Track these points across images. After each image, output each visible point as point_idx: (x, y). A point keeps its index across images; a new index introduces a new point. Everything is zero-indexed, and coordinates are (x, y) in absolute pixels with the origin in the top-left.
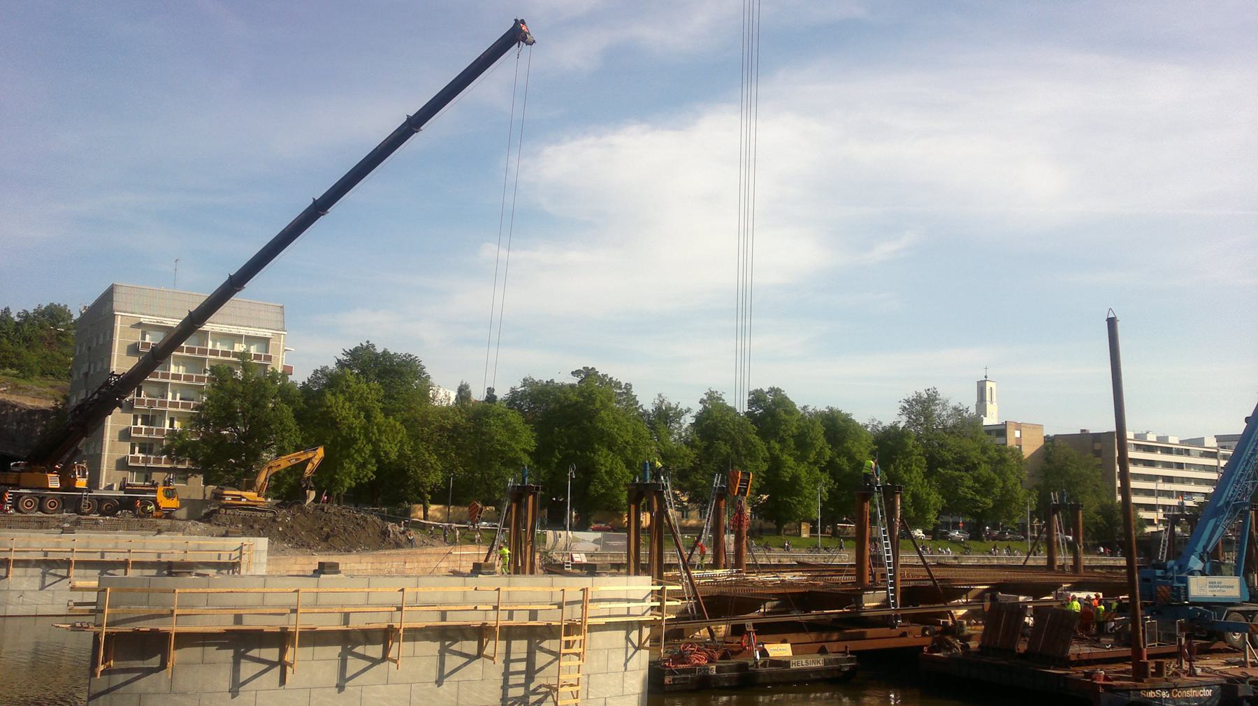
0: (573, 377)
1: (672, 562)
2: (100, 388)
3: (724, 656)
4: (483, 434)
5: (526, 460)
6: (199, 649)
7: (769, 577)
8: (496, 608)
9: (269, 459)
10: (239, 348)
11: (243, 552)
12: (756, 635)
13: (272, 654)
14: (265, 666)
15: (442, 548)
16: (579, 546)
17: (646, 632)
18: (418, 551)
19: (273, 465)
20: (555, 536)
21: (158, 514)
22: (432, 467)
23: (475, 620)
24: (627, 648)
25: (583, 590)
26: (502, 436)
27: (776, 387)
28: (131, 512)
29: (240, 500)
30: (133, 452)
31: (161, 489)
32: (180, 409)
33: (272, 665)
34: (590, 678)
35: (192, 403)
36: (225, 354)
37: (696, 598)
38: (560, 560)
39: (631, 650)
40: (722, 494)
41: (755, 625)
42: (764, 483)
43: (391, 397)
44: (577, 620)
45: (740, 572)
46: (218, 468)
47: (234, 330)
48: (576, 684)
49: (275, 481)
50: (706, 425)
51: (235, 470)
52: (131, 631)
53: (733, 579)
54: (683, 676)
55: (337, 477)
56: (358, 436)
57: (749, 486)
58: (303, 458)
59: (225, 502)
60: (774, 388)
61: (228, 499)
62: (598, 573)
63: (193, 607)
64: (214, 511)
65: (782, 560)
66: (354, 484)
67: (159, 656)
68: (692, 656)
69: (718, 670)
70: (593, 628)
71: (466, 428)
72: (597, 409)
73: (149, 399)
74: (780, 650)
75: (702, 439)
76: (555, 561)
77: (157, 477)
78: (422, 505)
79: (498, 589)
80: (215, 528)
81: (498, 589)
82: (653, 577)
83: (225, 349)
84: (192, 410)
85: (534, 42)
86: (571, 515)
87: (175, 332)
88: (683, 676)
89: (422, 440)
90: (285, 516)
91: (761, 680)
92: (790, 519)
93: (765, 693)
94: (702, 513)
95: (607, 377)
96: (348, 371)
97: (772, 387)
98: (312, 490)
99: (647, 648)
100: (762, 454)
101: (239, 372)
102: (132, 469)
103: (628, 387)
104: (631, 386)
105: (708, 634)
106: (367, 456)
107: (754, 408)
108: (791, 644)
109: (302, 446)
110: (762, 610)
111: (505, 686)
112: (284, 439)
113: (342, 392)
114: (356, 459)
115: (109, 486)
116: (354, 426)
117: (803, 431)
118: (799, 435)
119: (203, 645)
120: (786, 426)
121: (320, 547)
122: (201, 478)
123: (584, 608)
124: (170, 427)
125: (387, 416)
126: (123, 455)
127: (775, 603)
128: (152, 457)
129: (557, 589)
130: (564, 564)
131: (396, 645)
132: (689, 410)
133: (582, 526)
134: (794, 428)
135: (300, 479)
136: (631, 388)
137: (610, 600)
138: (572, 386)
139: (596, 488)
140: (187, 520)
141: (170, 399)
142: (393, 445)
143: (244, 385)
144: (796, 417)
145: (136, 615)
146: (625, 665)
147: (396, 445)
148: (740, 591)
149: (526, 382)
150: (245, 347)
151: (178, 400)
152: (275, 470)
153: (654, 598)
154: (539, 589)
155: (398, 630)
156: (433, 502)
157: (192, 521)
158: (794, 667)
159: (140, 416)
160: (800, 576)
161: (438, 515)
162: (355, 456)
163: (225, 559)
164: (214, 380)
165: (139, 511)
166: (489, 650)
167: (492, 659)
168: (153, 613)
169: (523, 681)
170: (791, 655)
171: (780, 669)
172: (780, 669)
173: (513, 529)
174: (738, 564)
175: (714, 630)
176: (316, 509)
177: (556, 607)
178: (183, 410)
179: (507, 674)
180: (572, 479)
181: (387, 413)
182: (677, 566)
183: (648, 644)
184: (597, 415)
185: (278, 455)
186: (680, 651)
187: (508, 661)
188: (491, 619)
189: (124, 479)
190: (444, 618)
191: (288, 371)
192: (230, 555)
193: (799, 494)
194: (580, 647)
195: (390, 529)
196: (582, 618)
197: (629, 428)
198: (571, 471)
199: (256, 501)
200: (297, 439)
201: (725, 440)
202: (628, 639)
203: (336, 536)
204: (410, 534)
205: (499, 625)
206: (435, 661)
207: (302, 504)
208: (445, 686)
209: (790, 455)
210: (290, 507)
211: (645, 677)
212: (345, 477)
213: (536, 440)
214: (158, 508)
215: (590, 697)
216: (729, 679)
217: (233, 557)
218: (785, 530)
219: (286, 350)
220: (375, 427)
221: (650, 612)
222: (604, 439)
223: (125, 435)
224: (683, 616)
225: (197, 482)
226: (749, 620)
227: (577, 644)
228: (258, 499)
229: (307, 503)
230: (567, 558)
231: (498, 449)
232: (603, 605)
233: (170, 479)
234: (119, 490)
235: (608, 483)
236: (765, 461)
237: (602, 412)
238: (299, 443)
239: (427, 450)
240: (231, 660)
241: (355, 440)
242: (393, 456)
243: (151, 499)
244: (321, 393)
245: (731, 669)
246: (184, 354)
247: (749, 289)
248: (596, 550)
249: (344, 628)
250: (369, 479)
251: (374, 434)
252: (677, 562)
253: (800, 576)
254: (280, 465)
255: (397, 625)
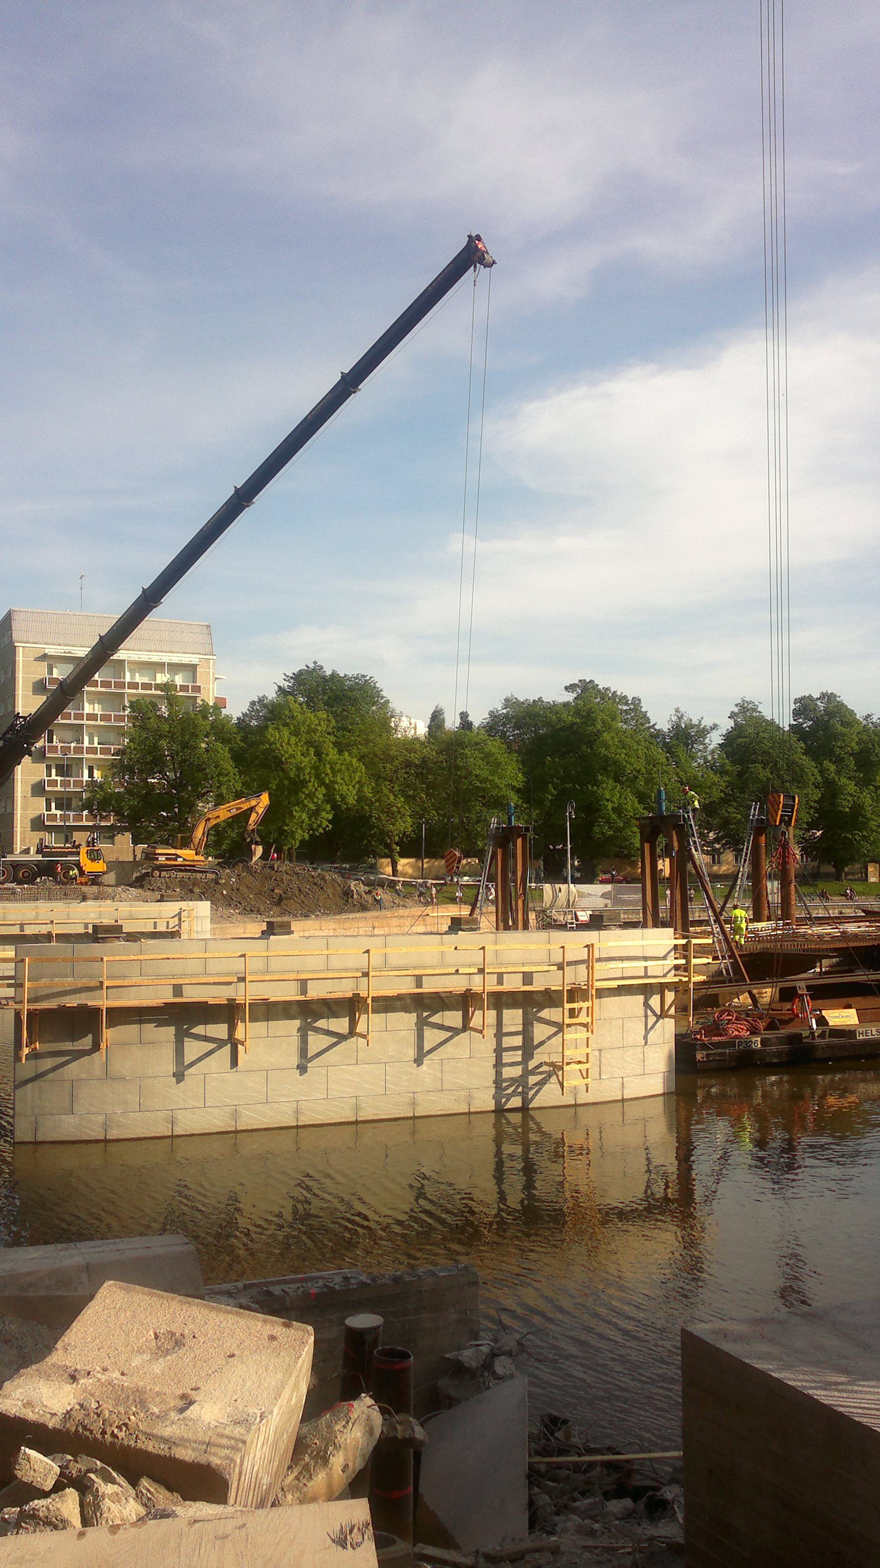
0: (567, 693)
1: (702, 918)
2: (5, 734)
3: (771, 1026)
4: (458, 768)
5: (514, 799)
6: (135, 1027)
7: (827, 930)
8: (481, 971)
9: (206, 810)
10: (162, 678)
11: (183, 919)
12: (811, 999)
13: (219, 1030)
14: (211, 1046)
15: (415, 909)
16: (585, 902)
17: (670, 996)
18: (388, 913)
19: (210, 816)
20: (554, 891)
21: (83, 880)
22: (399, 812)
23: (458, 985)
24: (646, 1016)
25: (587, 946)
26: (480, 769)
27: (829, 692)
28: (50, 878)
29: (176, 860)
30: (49, 808)
31: (83, 850)
32: (99, 756)
33: (221, 1043)
34: (603, 1054)
35: (112, 747)
36: (146, 686)
37: (732, 956)
38: (562, 919)
39: (652, 1019)
40: (761, 828)
41: (809, 988)
42: (816, 815)
43: (344, 729)
44: (582, 984)
45: (788, 924)
46: (147, 824)
47: (155, 657)
48: (585, 1061)
49: (215, 836)
50: (737, 745)
51: (167, 825)
52: (56, 1007)
53: (779, 932)
54: (719, 1051)
55: (286, 828)
56: (307, 778)
57: (795, 812)
58: (245, 806)
59: (158, 863)
60: (827, 693)
61: (162, 859)
62: (605, 926)
63: (124, 977)
64: (147, 874)
65: (844, 911)
66: (307, 837)
67: (90, 1036)
68: (729, 1026)
69: (763, 1042)
70: (601, 993)
71: (438, 762)
72: (598, 731)
73: (62, 745)
74: (843, 1016)
75: (734, 763)
76: (555, 921)
77: (80, 837)
78: (389, 860)
79: (483, 948)
80: (149, 893)
81: (483, 948)
82: (675, 930)
83: (146, 680)
84: (113, 755)
85: (494, 262)
86: (572, 863)
87: (86, 661)
88: (719, 1051)
89: (385, 779)
90: (229, 877)
91: (819, 1054)
92: (852, 860)
93: (825, 1071)
94: (738, 853)
95: (610, 690)
96: (290, 697)
97: (825, 692)
98: (258, 845)
99: (671, 1017)
100: (812, 779)
101: (163, 707)
102: (50, 829)
103: (637, 702)
104: (639, 700)
105: (750, 1001)
106: (320, 802)
107: (801, 720)
108: (857, 1010)
109: (243, 793)
110: (818, 970)
111: (499, 1064)
112: (221, 784)
113: (286, 725)
114: (307, 806)
115: (25, 850)
116: (303, 765)
117: (866, 747)
118: (861, 752)
119: (140, 1022)
120: (844, 741)
121: (272, 913)
122: (128, 836)
123: (590, 968)
124: (89, 777)
125: (340, 752)
126: (38, 813)
127: (834, 960)
128: (72, 814)
129: (555, 947)
130: (566, 924)
131: (364, 1017)
132: (715, 727)
133: (587, 876)
134: (854, 744)
135: (243, 833)
136: (640, 703)
137: (622, 959)
138: (566, 705)
139: (602, 830)
140: (117, 886)
141: (86, 744)
142: (350, 787)
143: (171, 722)
144: (856, 729)
145: (60, 990)
146: (645, 1038)
147: (354, 786)
148: (788, 947)
149: (508, 702)
150: (168, 676)
151: (96, 745)
152: (213, 822)
153: (677, 955)
154: (532, 947)
155: (366, 999)
156: (402, 855)
157: (122, 887)
158: (861, 1037)
159: (53, 766)
160: (867, 927)
161: (410, 871)
162: (306, 801)
163: (161, 928)
164: (136, 718)
165: (60, 877)
166: (476, 1020)
167: (481, 1032)
168: (80, 985)
169: (519, 1059)
170: (857, 1022)
171: (842, 1040)
172: (842, 1040)
173: (500, 884)
174: (786, 914)
175: (757, 996)
176: (264, 867)
177: (555, 968)
178: (103, 756)
179: (499, 1051)
180: (571, 819)
181: (341, 748)
182: (707, 923)
183: (672, 1011)
184: (599, 738)
185: (217, 805)
186: (714, 1021)
187: (500, 1035)
188: (477, 984)
189: (41, 840)
190: (419, 985)
191: (220, 703)
192: (168, 922)
193: (864, 826)
194: (588, 1016)
195: (353, 888)
196: (588, 981)
197: (640, 752)
198: (569, 809)
199: (193, 861)
200: (236, 785)
201: (762, 762)
202: (646, 1005)
203: (290, 898)
204: (377, 894)
205: (486, 992)
206: (412, 1037)
207: (247, 862)
208: (424, 1067)
209: (849, 778)
210: (233, 867)
211: (670, 1053)
212: (297, 829)
213: (524, 774)
214: (82, 872)
215: (603, 1077)
216: (780, 1054)
217: (170, 926)
218: (847, 874)
219: (216, 679)
220: (328, 766)
221: (673, 972)
222: (609, 768)
223: (38, 789)
224: (716, 979)
225: (125, 840)
226: (801, 982)
227: (584, 1013)
228: (196, 858)
229: (253, 861)
230: (570, 917)
231: (478, 787)
232: (612, 964)
233: (93, 839)
234: (37, 853)
235: (616, 823)
236: (816, 787)
237: (605, 735)
238: (239, 789)
239: (391, 791)
240: (173, 1038)
241: (304, 783)
242: (352, 800)
243: (74, 862)
244: (262, 729)
245: (781, 1041)
246: (99, 689)
247: (785, 578)
248: (606, 906)
249: (302, 998)
250: (324, 829)
251: (327, 775)
252: (707, 918)
253: (867, 927)
254: (218, 817)
255: (364, 994)
